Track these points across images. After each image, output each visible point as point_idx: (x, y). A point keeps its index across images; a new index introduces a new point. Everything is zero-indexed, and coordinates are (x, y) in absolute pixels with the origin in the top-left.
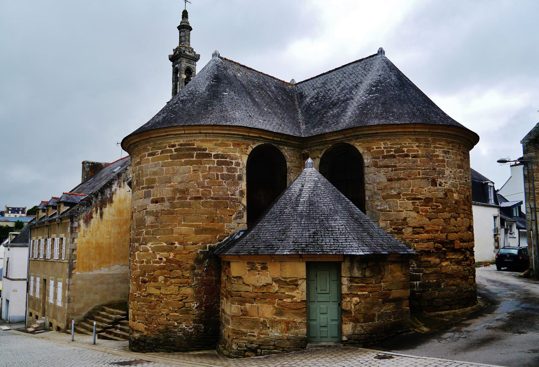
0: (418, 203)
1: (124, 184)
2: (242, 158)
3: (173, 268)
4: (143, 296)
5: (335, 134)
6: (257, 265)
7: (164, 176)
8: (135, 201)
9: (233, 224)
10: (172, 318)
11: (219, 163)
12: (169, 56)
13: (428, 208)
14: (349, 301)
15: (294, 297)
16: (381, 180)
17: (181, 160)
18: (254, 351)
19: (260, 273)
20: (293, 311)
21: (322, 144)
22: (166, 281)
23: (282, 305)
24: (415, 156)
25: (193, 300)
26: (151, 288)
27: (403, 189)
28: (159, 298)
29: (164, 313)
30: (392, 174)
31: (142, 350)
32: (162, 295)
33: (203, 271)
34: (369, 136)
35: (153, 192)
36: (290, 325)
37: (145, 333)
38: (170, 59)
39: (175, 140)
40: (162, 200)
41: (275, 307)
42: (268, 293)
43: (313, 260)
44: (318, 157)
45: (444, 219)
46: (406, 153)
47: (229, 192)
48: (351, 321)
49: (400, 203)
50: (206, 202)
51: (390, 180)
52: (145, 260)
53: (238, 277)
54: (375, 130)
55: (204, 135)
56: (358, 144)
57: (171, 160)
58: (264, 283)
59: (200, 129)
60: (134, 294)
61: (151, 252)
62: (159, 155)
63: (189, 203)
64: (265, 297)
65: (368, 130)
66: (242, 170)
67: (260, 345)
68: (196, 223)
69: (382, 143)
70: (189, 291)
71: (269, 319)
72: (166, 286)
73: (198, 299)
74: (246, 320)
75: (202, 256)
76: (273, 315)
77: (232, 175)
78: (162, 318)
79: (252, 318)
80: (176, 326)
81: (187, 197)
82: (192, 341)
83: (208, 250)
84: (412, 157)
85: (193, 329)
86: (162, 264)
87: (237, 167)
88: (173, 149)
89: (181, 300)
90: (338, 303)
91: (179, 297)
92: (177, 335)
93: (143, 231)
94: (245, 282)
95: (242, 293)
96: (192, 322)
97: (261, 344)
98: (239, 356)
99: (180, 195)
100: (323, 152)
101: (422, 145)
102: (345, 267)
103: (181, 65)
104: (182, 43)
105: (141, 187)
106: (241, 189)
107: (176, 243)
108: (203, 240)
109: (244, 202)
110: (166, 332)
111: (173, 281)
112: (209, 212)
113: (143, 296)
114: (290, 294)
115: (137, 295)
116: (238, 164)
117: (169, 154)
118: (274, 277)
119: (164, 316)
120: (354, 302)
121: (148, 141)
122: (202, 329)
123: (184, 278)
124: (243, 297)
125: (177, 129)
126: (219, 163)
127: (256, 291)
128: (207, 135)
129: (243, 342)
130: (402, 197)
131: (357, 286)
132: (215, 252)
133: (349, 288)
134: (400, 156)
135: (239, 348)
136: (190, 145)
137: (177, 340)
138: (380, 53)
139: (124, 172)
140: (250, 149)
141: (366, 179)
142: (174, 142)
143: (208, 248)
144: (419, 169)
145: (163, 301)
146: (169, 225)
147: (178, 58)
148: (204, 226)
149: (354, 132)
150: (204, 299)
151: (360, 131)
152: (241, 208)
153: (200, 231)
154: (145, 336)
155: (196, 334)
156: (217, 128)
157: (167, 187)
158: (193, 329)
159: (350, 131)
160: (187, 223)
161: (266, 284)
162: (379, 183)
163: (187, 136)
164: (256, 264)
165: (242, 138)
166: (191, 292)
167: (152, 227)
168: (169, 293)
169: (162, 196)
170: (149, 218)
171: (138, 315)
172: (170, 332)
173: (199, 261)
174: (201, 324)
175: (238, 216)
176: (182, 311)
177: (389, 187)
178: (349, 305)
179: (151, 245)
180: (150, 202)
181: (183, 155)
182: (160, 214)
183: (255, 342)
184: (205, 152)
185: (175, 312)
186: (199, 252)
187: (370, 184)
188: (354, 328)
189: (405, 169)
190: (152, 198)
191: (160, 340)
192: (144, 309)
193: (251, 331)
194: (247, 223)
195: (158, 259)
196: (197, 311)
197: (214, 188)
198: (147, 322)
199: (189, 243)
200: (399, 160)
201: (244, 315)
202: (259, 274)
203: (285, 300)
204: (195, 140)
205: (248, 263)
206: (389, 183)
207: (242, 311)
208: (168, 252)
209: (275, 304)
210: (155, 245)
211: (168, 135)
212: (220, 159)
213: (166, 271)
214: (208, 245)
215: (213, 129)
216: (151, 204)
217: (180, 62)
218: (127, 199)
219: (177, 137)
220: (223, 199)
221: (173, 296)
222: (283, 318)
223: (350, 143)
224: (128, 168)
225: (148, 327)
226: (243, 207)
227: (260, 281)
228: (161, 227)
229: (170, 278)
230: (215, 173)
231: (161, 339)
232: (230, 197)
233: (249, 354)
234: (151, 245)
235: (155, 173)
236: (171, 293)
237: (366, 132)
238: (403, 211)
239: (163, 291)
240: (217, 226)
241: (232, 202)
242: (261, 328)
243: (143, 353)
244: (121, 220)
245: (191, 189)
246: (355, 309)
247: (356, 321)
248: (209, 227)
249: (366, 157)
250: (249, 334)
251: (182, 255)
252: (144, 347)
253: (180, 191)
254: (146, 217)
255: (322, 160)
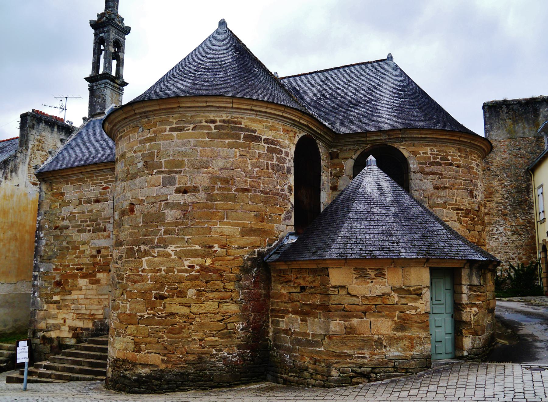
0: (461, 214)
1: (11, 175)
2: (291, 147)
3: (210, 279)
4: (158, 317)
5: (379, 134)
6: (369, 272)
7: (198, 158)
8: (139, 190)
9: (282, 226)
10: (208, 343)
11: (270, 150)
12: (91, 21)
13: (468, 219)
14: (469, 312)
15: (418, 308)
16: (428, 187)
17: (224, 140)
18: (367, 377)
19: (374, 281)
20: (418, 325)
21: (358, 144)
22: (199, 294)
23: (404, 318)
24: (458, 166)
25: (238, 319)
26: (175, 305)
27: (448, 198)
28: (188, 319)
29: (196, 338)
30: (439, 182)
31: (155, 390)
32: (192, 315)
33: (251, 283)
34: (416, 140)
35: (179, 178)
36: (415, 341)
37: (163, 366)
38: (91, 25)
39: (216, 114)
40: (195, 189)
41: (395, 321)
42: (383, 305)
43: (437, 266)
44: (352, 158)
45: (478, 232)
46: (450, 161)
47: (279, 186)
48: (471, 333)
49: (447, 213)
50: (255, 196)
51: (436, 188)
52: (163, 268)
53: (339, 286)
54: (425, 134)
55: (254, 113)
56: (403, 147)
57: (209, 139)
58: (379, 292)
59: (252, 105)
60: (138, 314)
61: (174, 257)
62: (190, 131)
63: (234, 195)
64: (380, 310)
65: (417, 133)
66: (289, 163)
67: (373, 368)
68: (243, 222)
69: (429, 148)
70: (233, 308)
71: (387, 336)
72: (200, 302)
73: (244, 318)
74: (353, 339)
75: (249, 263)
76: (392, 331)
77: (281, 166)
78: (193, 344)
79: (362, 335)
80: (214, 354)
81: (232, 188)
82: (236, 373)
83: (256, 256)
84: (455, 167)
85: (237, 357)
86: (193, 273)
87: (286, 157)
88: (212, 126)
89: (220, 321)
90: (451, 315)
91: (219, 317)
92: (216, 366)
93: (161, 230)
94: (350, 292)
95: (346, 306)
96: (235, 348)
97: (375, 367)
98: (342, 384)
99: (221, 184)
100: (359, 153)
101: (463, 155)
102: (465, 273)
103: (109, 35)
104: (110, 9)
105: (155, 171)
106: (289, 184)
107: (216, 245)
108: (251, 244)
109: (292, 200)
110: (199, 363)
111: (211, 295)
112: (258, 208)
113: (158, 317)
114: (413, 304)
115: (146, 316)
116: (287, 154)
117: (206, 131)
118: (393, 285)
119: (196, 343)
120: (474, 312)
121: (174, 112)
122: (249, 357)
123: (226, 291)
124: (348, 311)
125: (224, 100)
126: (270, 150)
127: (367, 302)
128: (259, 113)
129: (348, 367)
130: (448, 206)
131: (475, 295)
132: (264, 259)
133: (469, 297)
134: (445, 164)
135: (341, 375)
136: (235, 123)
137: (216, 373)
138: (390, 58)
139: (13, 160)
140: (297, 139)
141: (413, 185)
142: (214, 117)
143: (256, 253)
144: (461, 179)
145: (193, 323)
146: (205, 223)
147: (105, 26)
148: (252, 226)
149: (401, 134)
150: (252, 318)
151: (408, 134)
152: (289, 207)
153: (247, 232)
154: (161, 370)
155: (242, 363)
156: (273, 107)
157: (203, 174)
158: (237, 357)
159: (398, 133)
160: (231, 221)
161: (382, 293)
162: (426, 190)
163: (233, 112)
164: (368, 270)
165: (292, 123)
166: (235, 309)
167: (177, 224)
168: (204, 311)
169: (195, 185)
170: (172, 212)
171: (146, 344)
172: (205, 362)
173: (245, 270)
174: (248, 350)
175: (287, 217)
176: (223, 334)
177: (435, 195)
178: (469, 316)
179: (175, 247)
180: (174, 191)
181: (227, 134)
182: (190, 208)
183: (367, 365)
184: (254, 134)
185: (213, 336)
186: (246, 258)
187: (416, 190)
188: (474, 341)
189: (450, 178)
190: (177, 186)
191: (189, 374)
192: (161, 334)
193: (360, 352)
194: (295, 226)
195: (186, 267)
196: (243, 333)
197: (264, 179)
198: (166, 351)
199: (233, 246)
200: (445, 168)
201: (349, 333)
202: (372, 282)
203: (408, 312)
204: (242, 118)
205: (356, 269)
206: (436, 191)
207: (345, 328)
208: (203, 257)
209: (394, 318)
210: (182, 248)
211: (207, 106)
212: (270, 145)
213: (200, 283)
214: (256, 250)
215: (267, 108)
216: (174, 194)
217: (109, 31)
218: (14, 195)
219: (220, 111)
220: (273, 194)
221: (209, 315)
222: (406, 334)
223: (393, 145)
224: (18, 155)
225: (168, 357)
226: (291, 206)
227: (373, 291)
228: (192, 225)
229: (206, 291)
230: (265, 161)
231: (191, 373)
232: (280, 192)
233: (359, 381)
234: (175, 247)
235: (182, 154)
236: (206, 311)
237: (415, 136)
238: (449, 221)
239: (194, 309)
240: (266, 226)
241: (281, 199)
242: (375, 347)
243: (159, 394)
244: (5, 223)
245: (236, 179)
246: (475, 320)
247: (475, 333)
248: (258, 227)
249: (412, 161)
250: (356, 355)
251: (224, 262)
252: (160, 386)
253: (222, 180)
254: (166, 211)
255: (356, 161)
